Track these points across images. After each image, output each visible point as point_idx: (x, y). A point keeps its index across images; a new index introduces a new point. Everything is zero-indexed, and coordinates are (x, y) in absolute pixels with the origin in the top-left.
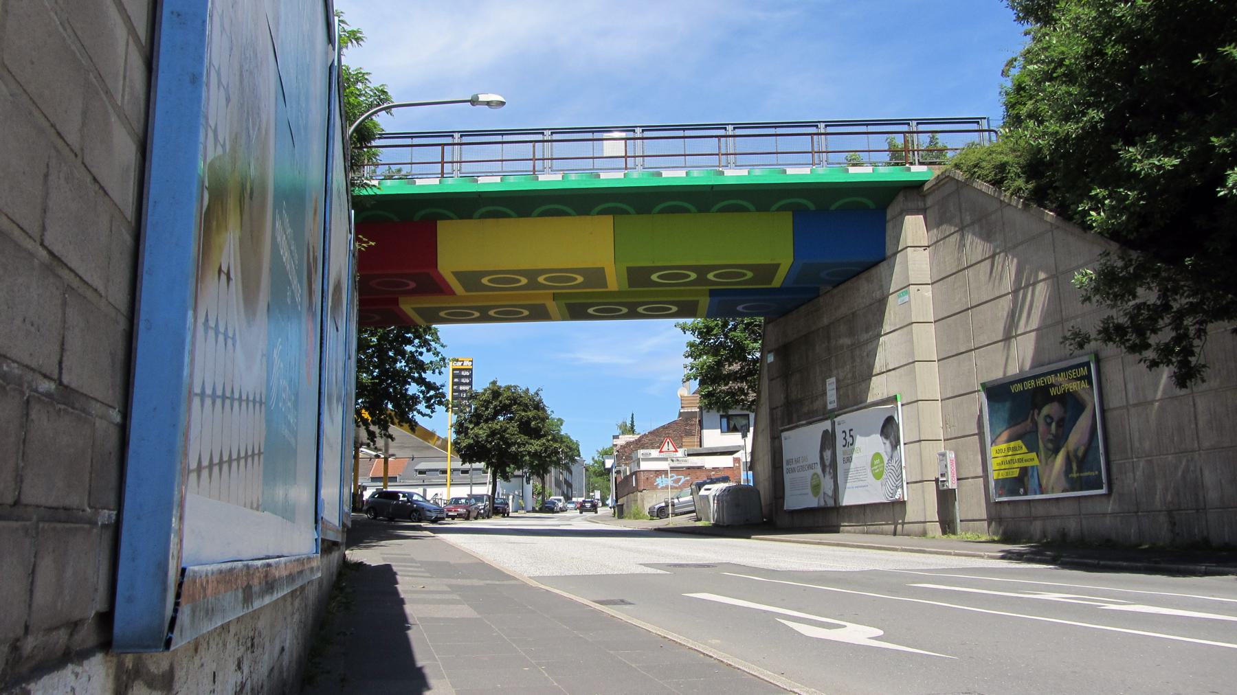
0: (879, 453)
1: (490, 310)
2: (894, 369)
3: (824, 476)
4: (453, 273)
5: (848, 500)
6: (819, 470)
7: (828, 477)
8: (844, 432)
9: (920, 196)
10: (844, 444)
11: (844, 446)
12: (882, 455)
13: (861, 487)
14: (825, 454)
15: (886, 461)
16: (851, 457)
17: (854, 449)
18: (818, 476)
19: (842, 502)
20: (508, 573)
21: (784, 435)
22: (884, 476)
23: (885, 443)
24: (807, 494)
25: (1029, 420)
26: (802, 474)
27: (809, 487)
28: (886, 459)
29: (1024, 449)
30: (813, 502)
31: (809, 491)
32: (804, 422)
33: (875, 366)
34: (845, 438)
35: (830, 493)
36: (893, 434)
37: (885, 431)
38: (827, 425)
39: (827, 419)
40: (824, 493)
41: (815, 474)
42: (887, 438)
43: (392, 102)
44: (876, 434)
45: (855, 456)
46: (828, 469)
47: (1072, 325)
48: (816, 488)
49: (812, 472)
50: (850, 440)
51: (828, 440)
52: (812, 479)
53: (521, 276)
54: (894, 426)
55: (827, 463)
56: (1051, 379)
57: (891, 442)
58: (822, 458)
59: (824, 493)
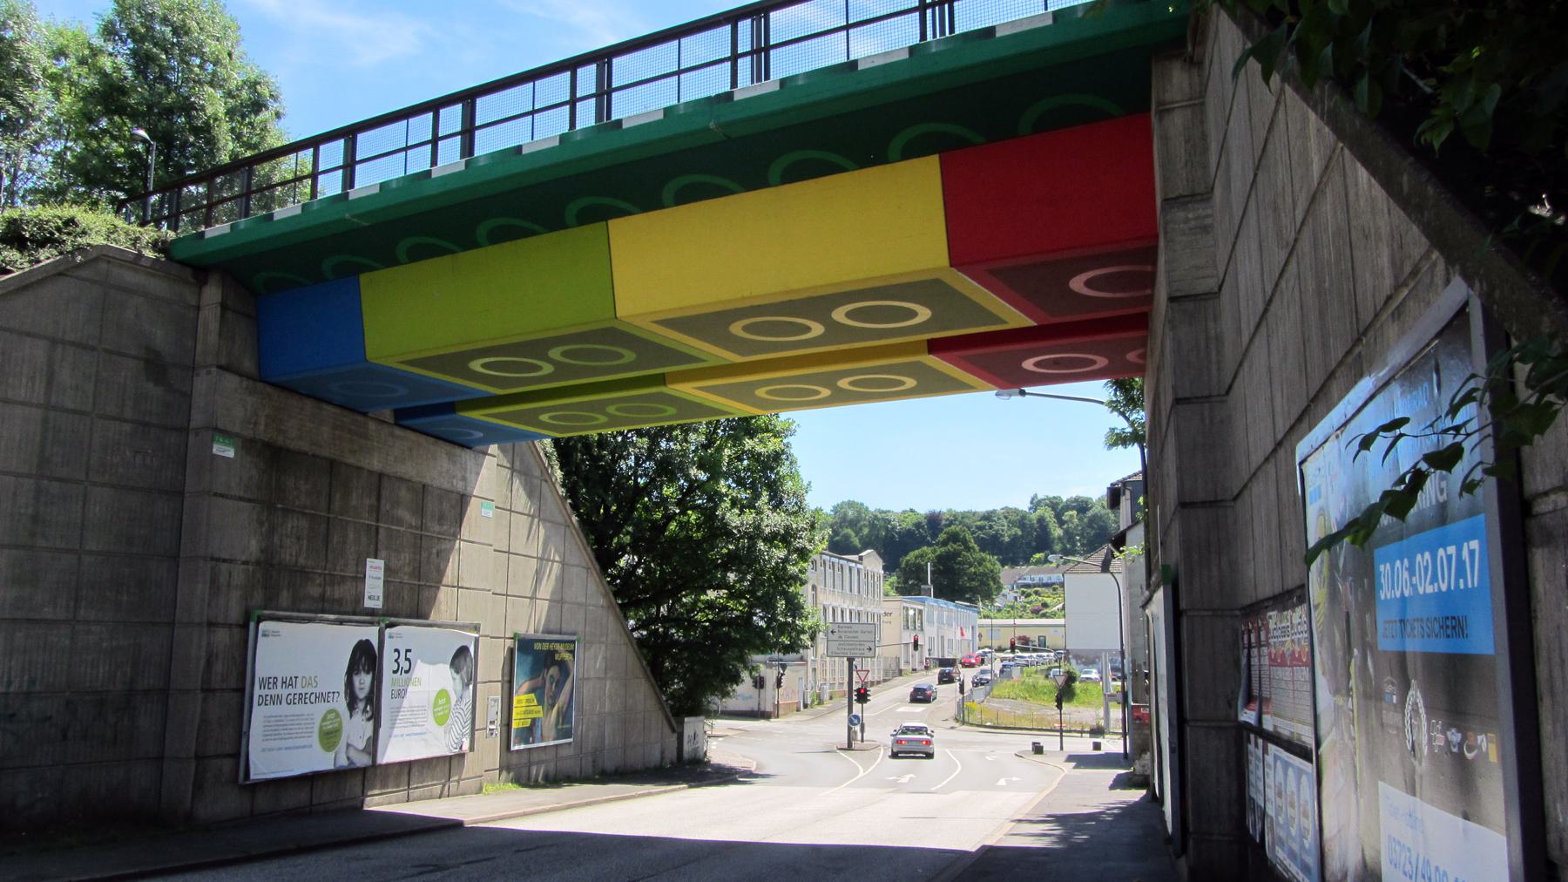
0: (446, 691)
2: (467, 588)
3: (351, 716)
4: (1112, 787)
5: (392, 753)
6: (341, 704)
7: (359, 717)
8: (397, 650)
9: (1080, 703)
10: (395, 669)
11: (395, 672)
12: (450, 693)
13: (416, 734)
14: (356, 680)
15: (453, 702)
16: (406, 691)
17: (410, 679)
18: (338, 715)
19: (384, 754)
22: (449, 722)
23: (454, 679)
25: (541, 677)
26: (299, 708)
28: (454, 698)
29: (535, 702)
30: (324, 761)
32: (332, 617)
33: (446, 574)
34: (396, 661)
36: (465, 668)
37: (456, 662)
38: (370, 633)
39: (371, 623)
40: (348, 745)
42: (457, 672)
44: (445, 663)
45: (410, 689)
46: (361, 705)
47: (1048, 600)
48: (330, 737)
49: (321, 708)
50: (405, 665)
51: (366, 658)
52: (324, 719)
53: (742, 339)
54: (468, 659)
55: (362, 695)
56: (559, 647)
57: (462, 679)
58: (349, 684)
59: (348, 745)
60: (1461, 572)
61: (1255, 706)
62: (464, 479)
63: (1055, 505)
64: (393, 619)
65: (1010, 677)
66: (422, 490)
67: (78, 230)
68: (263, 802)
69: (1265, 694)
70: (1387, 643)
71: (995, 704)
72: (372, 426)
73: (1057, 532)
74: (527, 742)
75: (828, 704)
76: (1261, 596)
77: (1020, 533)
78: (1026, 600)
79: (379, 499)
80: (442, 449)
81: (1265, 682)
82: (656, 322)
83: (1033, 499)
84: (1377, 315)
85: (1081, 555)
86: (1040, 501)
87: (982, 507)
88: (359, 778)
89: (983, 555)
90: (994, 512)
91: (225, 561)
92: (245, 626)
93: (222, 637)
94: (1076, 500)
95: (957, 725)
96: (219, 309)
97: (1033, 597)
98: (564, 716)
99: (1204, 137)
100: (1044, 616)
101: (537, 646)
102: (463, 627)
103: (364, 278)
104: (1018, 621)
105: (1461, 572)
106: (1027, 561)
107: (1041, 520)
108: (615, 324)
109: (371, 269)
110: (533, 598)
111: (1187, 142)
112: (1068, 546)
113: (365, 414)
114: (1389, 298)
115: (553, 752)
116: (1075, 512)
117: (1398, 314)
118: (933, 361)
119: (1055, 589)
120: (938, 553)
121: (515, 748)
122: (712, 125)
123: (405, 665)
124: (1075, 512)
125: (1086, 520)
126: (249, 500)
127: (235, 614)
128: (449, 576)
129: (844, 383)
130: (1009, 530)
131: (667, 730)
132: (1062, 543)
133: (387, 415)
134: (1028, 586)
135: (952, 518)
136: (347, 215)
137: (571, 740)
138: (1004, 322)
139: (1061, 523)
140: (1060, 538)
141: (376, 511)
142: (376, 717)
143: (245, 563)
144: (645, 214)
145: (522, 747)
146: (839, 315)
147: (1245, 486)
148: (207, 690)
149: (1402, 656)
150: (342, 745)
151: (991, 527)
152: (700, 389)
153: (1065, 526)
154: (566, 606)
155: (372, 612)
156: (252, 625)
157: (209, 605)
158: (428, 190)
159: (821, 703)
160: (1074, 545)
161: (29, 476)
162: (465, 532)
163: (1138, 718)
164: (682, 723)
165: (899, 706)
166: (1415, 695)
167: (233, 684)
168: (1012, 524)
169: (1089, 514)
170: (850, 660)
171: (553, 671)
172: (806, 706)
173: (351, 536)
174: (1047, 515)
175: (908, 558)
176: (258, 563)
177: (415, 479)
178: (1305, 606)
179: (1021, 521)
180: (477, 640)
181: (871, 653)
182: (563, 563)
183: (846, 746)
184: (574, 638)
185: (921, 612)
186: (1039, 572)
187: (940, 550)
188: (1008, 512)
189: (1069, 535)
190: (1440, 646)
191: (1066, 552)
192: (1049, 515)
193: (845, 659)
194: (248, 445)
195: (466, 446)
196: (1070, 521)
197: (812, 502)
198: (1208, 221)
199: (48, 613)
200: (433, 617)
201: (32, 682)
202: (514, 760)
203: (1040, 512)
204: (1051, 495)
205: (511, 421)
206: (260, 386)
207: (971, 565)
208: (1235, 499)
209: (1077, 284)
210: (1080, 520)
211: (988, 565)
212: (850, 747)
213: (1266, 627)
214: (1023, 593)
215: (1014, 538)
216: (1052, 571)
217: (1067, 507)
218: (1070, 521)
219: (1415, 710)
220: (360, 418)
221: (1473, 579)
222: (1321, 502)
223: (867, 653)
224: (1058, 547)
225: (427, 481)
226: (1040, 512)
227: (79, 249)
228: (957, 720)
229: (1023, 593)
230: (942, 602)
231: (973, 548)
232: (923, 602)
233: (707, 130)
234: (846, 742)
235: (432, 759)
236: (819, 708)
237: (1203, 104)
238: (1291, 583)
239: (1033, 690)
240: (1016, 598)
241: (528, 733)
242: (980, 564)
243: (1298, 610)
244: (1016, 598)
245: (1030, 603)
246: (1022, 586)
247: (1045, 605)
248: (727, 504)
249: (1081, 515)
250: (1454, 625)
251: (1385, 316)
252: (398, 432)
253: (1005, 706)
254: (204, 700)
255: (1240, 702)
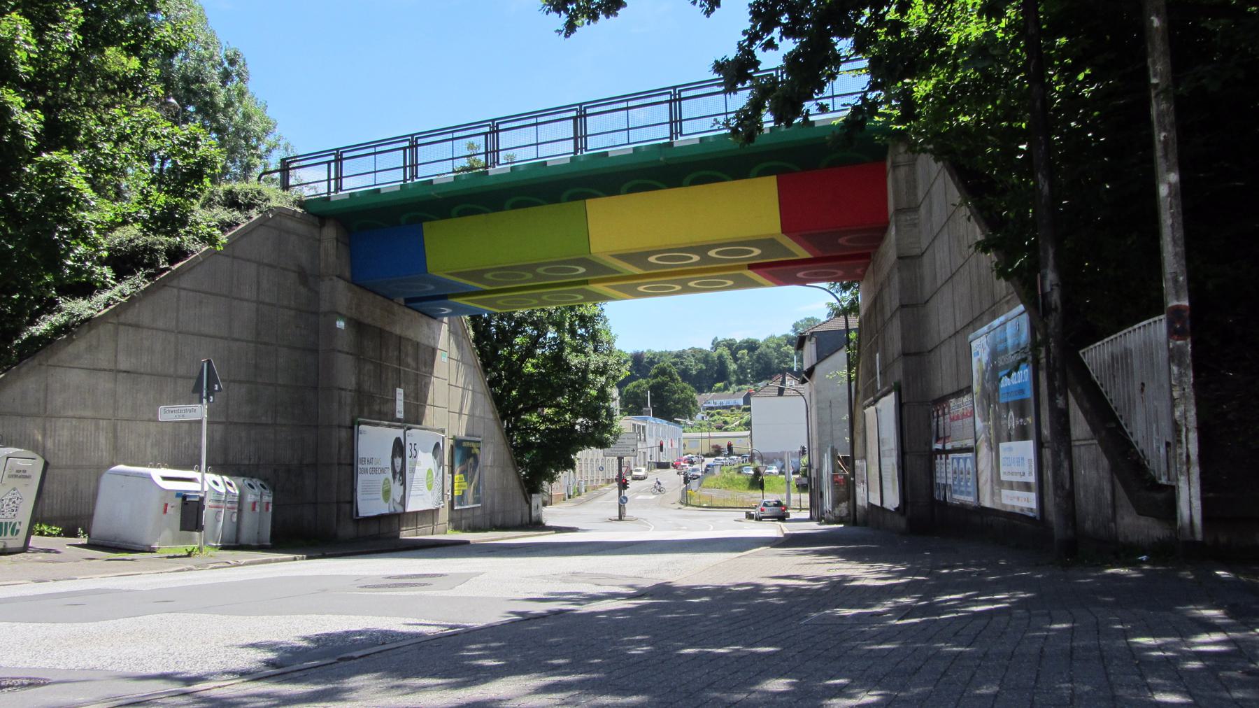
1: (759, 255)
5: (410, 508)
6: (390, 475)
7: (398, 483)
14: (395, 460)
20: (212, 582)
21: (362, 427)
24: (378, 499)
27: (381, 492)
31: (380, 495)
32: (386, 423)
35: (398, 500)
40: (394, 500)
41: (386, 479)
43: (817, 104)
45: (417, 467)
46: (398, 476)
47: (728, 419)
48: (387, 493)
49: (383, 476)
50: (414, 452)
51: (399, 448)
55: (398, 470)
56: (473, 445)
59: (394, 500)
60: (1023, 378)
61: (942, 441)
62: (434, 338)
63: (730, 345)
64: (409, 425)
65: (713, 473)
66: (417, 345)
67: (264, 198)
69: (947, 434)
70: (1003, 400)
71: (706, 492)
72: (396, 307)
73: (733, 367)
74: (461, 505)
75: (584, 495)
76: (945, 393)
77: (704, 367)
78: (711, 419)
79: (400, 352)
80: (424, 320)
81: (947, 430)
82: (613, 256)
83: (714, 341)
84: (1000, 300)
85: (751, 384)
86: (719, 343)
87: (675, 348)
88: (396, 521)
89: (685, 384)
90: (684, 351)
92: (352, 428)
94: (747, 341)
95: (682, 506)
96: (335, 241)
97: (716, 417)
98: (477, 489)
99: (915, 180)
100: (726, 430)
101: (464, 444)
102: (437, 431)
103: (426, 225)
104: (712, 434)
105: (1023, 378)
106: (710, 389)
107: (720, 357)
108: (587, 257)
109: (431, 220)
110: (460, 413)
111: (906, 182)
112: (741, 377)
113: (392, 300)
114: (1004, 297)
115: (471, 512)
116: (745, 351)
117: (1008, 302)
118: (751, 274)
119: (732, 411)
120: (651, 383)
121: (456, 508)
122: (661, 159)
123: (414, 452)
124: (745, 351)
125: (755, 357)
126: (351, 354)
127: (348, 423)
128: (429, 401)
129: (692, 284)
130: (696, 364)
131: (524, 502)
132: (737, 375)
133: (402, 301)
134: (712, 408)
135: (652, 356)
136: (433, 193)
137: (479, 505)
138: (797, 256)
139: (736, 360)
140: (735, 372)
141: (399, 360)
142: (404, 483)
143: (350, 391)
144: (607, 198)
145: (459, 508)
146: (712, 253)
147: (936, 347)
148: (339, 464)
149: (1007, 404)
150: (391, 500)
151: (682, 363)
152: (609, 287)
153: (739, 362)
154: (475, 418)
155: (399, 420)
156: (356, 426)
158: (486, 182)
159: (580, 494)
160: (746, 376)
161: (252, 342)
162: (435, 373)
163: (837, 482)
164: (531, 498)
165: (637, 495)
166: (1011, 413)
167: (349, 461)
168: (699, 360)
169: (757, 352)
170: (620, 459)
171: (471, 460)
172: (569, 497)
173: (390, 374)
174: (724, 353)
175: (628, 388)
176: (355, 390)
177: (415, 339)
178: (970, 395)
179: (705, 358)
180: (443, 438)
181: (635, 453)
182: (473, 391)
183: (618, 518)
184: (480, 439)
185: (644, 427)
186: (721, 398)
187: (652, 382)
188: (695, 352)
189: (742, 369)
190: (1018, 397)
191: (739, 382)
192: (726, 353)
193: (616, 458)
194: (351, 322)
195: (434, 318)
196: (743, 358)
197: (618, 345)
198: (916, 221)
199: (264, 420)
200: (424, 424)
201: (259, 459)
202: (455, 515)
203: (719, 351)
204: (728, 338)
205: (483, 305)
206: (353, 286)
207: (675, 393)
208: (930, 351)
209: (842, 241)
210: (751, 357)
211: (689, 392)
212: (620, 519)
213: (949, 407)
214: (708, 414)
215: (700, 372)
216: (729, 397)
217: (740, 347)
218: (743, 358)
219: (1011, 418)
220: (391, 302)
221: (1026, 379)
222: (979, 357)
223: (631, 453)
224: (733, 378)
225: (419, 340)
226: (719, 351)
227: (270, 209)
228: (682, 503)
229: (708, 414)
230: (658, 420)
231: (677, 379)
232: (645, 420)
233: (659, 161)
234: (618, 515)
235: (427, 510)
236: (578, 498)
237: (914, 164)
238: (963, 385)
239: (731, 482)
240: (703, 418)
241: (462, 498)
242: (682, 392)
243: (966, 397)
244: (703, 418)
245: (714, 421)
246: (707, 409)
247: (726, 423)
248: (568, 350)
249: (751, 353)
250: (1022, 391)
251: (1004, 301)
252: (407, 310)
253: (714, 493)
255: (933, 441)
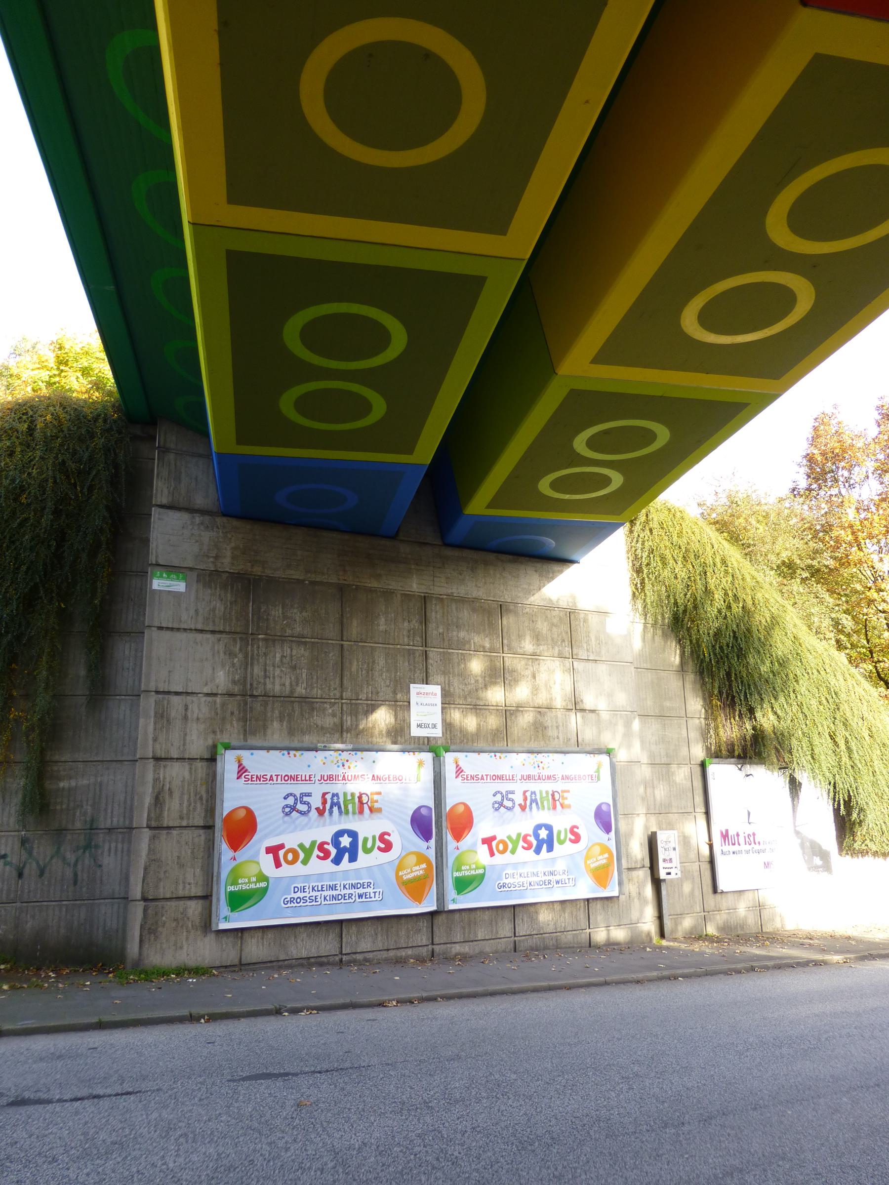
68: (255, 950)
91: (177, 693)
93: (176, 773)
126: (213, 632)
157: (155, 740)
254: (153, 838)
